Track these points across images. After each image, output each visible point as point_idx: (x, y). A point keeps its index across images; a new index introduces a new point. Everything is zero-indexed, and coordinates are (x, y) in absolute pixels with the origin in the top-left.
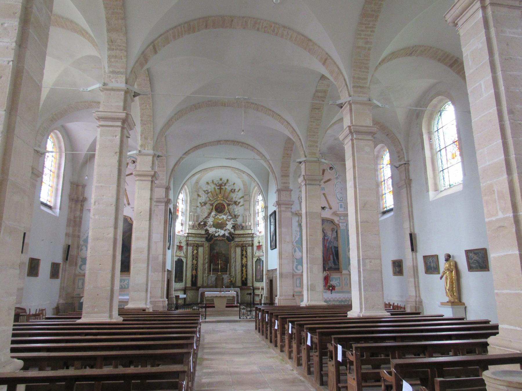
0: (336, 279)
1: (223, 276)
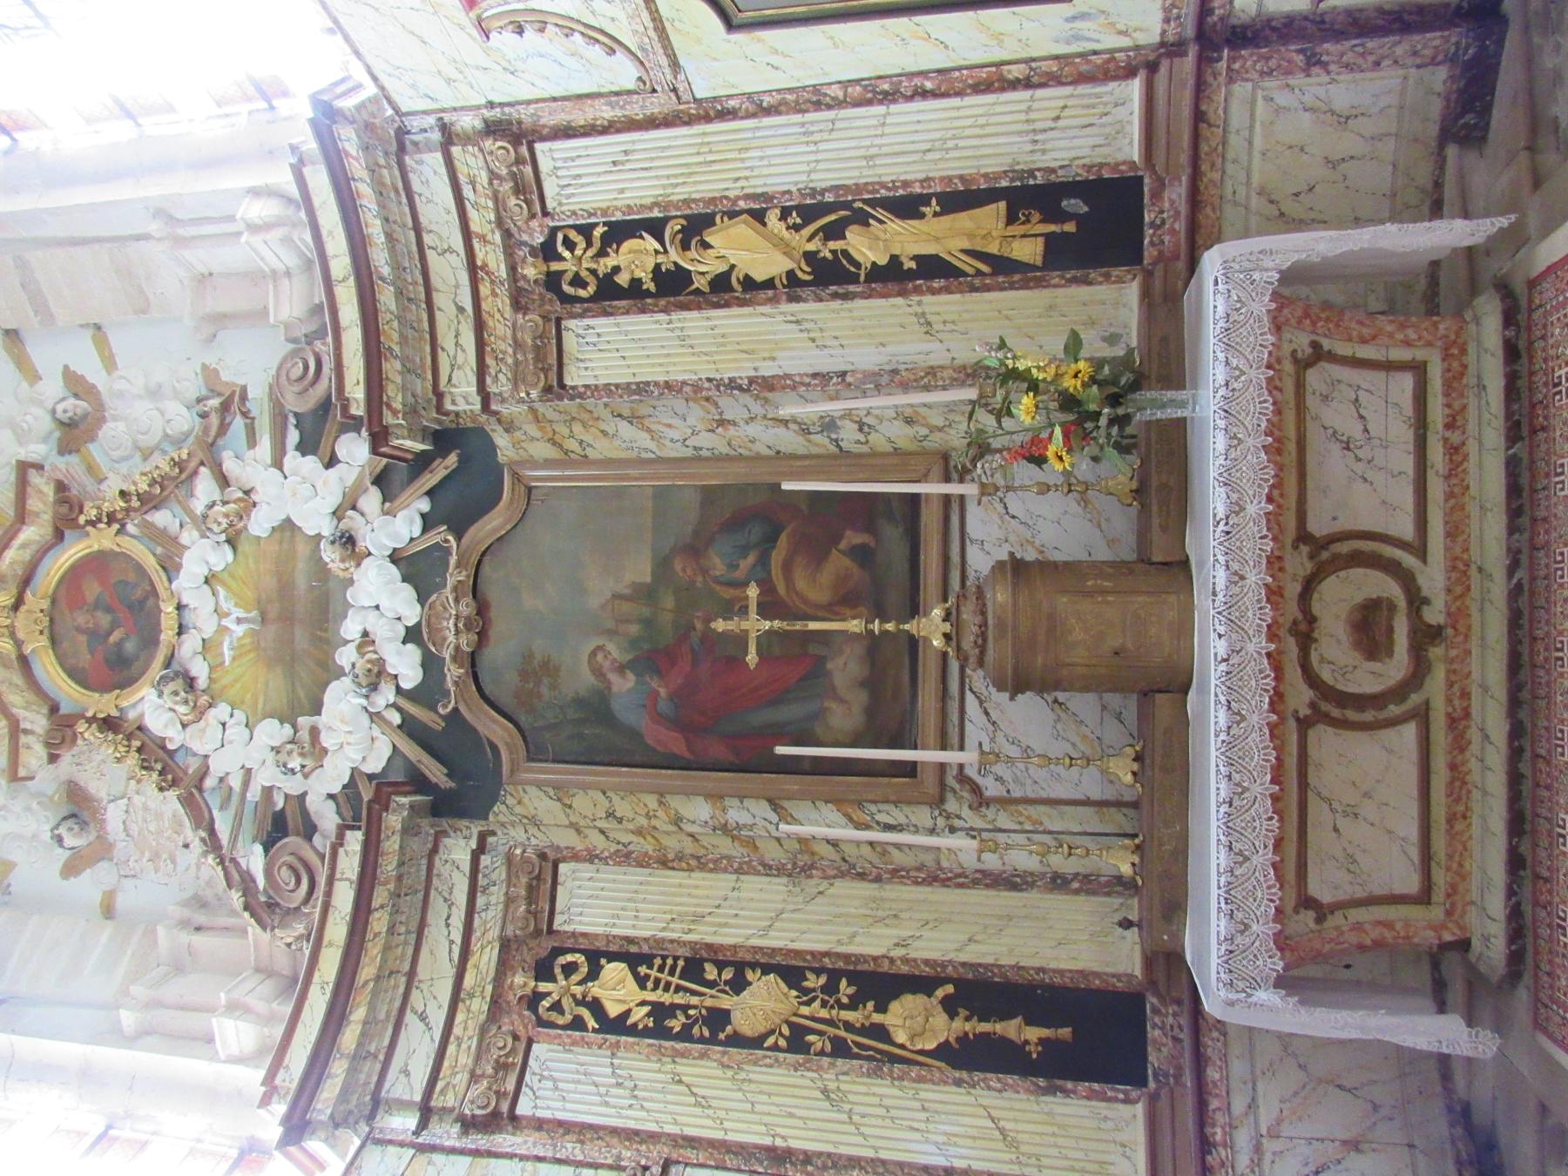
1: (980, 562)
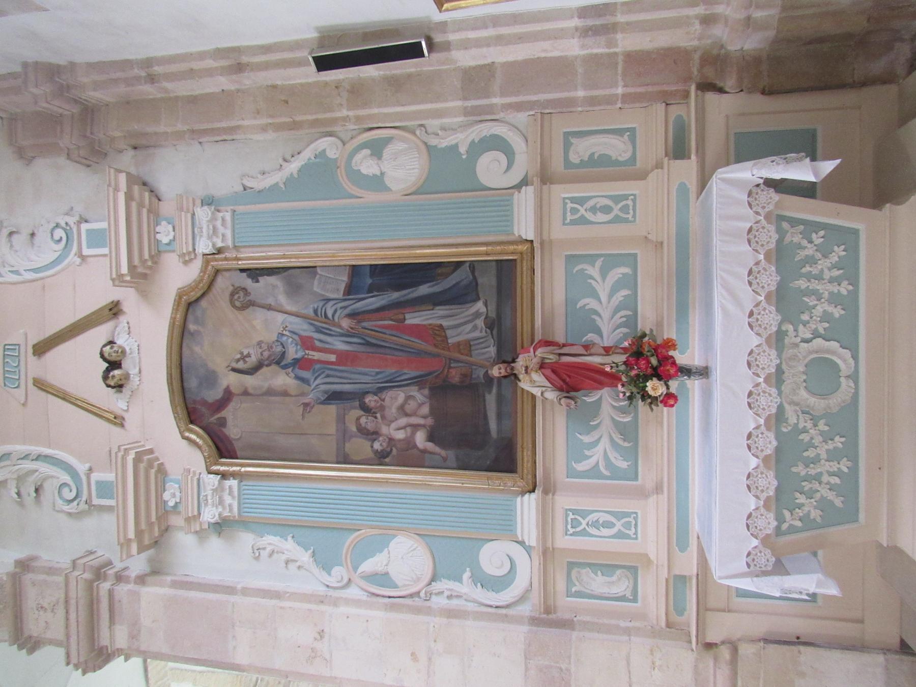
0: (579, 284)
